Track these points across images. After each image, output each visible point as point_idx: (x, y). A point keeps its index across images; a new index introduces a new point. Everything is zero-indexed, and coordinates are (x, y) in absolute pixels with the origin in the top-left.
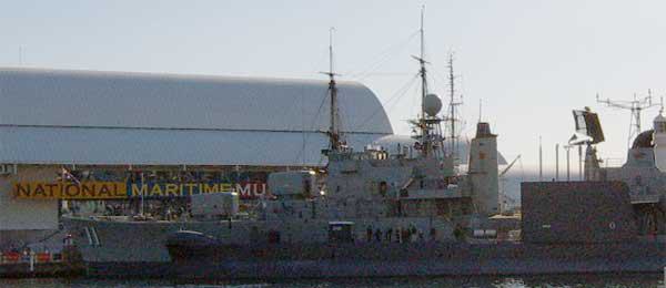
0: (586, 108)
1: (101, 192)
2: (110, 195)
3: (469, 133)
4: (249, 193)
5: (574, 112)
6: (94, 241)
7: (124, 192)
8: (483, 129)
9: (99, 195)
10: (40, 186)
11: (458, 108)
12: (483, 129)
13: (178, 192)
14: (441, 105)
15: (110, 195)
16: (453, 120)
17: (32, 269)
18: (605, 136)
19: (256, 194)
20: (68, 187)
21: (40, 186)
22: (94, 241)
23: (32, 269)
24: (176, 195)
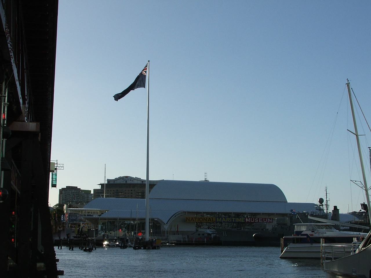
0: (364, 203)
1: (191, 220)
2: (194, 221)
3: (331, 210)
4: (250, 221)
5: (361, 204)
6: (225, 235)
7: (215, 220)
8: (335, 207)
9: (208, 221)
10: (192, 218)
11: (328, 202)
12: (335, 207)
13: (230, 220)
14: (323, 199)
15: (194, 221)
16: (327, 205)
17: (205, 242)
18: (93, 190)
19: (252, 221)
20: (200, 218)
21: (192, 218)
22: (225, 235)
23: (194, 242)
24: (229, 221)
